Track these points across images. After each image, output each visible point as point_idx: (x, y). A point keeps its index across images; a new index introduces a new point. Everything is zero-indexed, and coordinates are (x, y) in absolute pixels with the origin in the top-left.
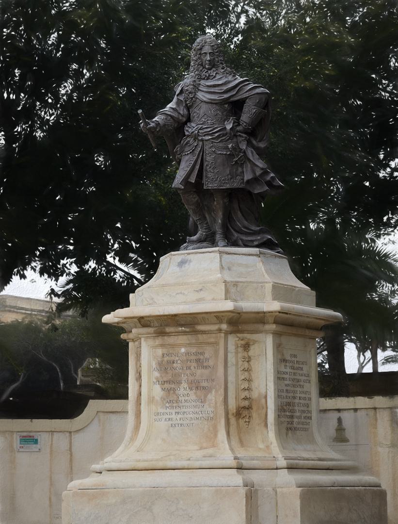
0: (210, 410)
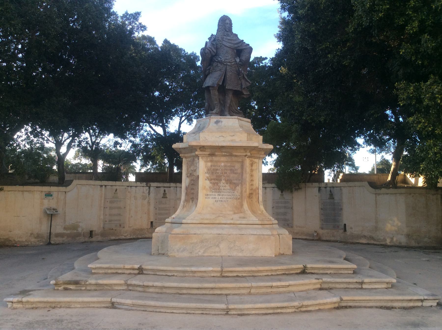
0: (237, 194)
